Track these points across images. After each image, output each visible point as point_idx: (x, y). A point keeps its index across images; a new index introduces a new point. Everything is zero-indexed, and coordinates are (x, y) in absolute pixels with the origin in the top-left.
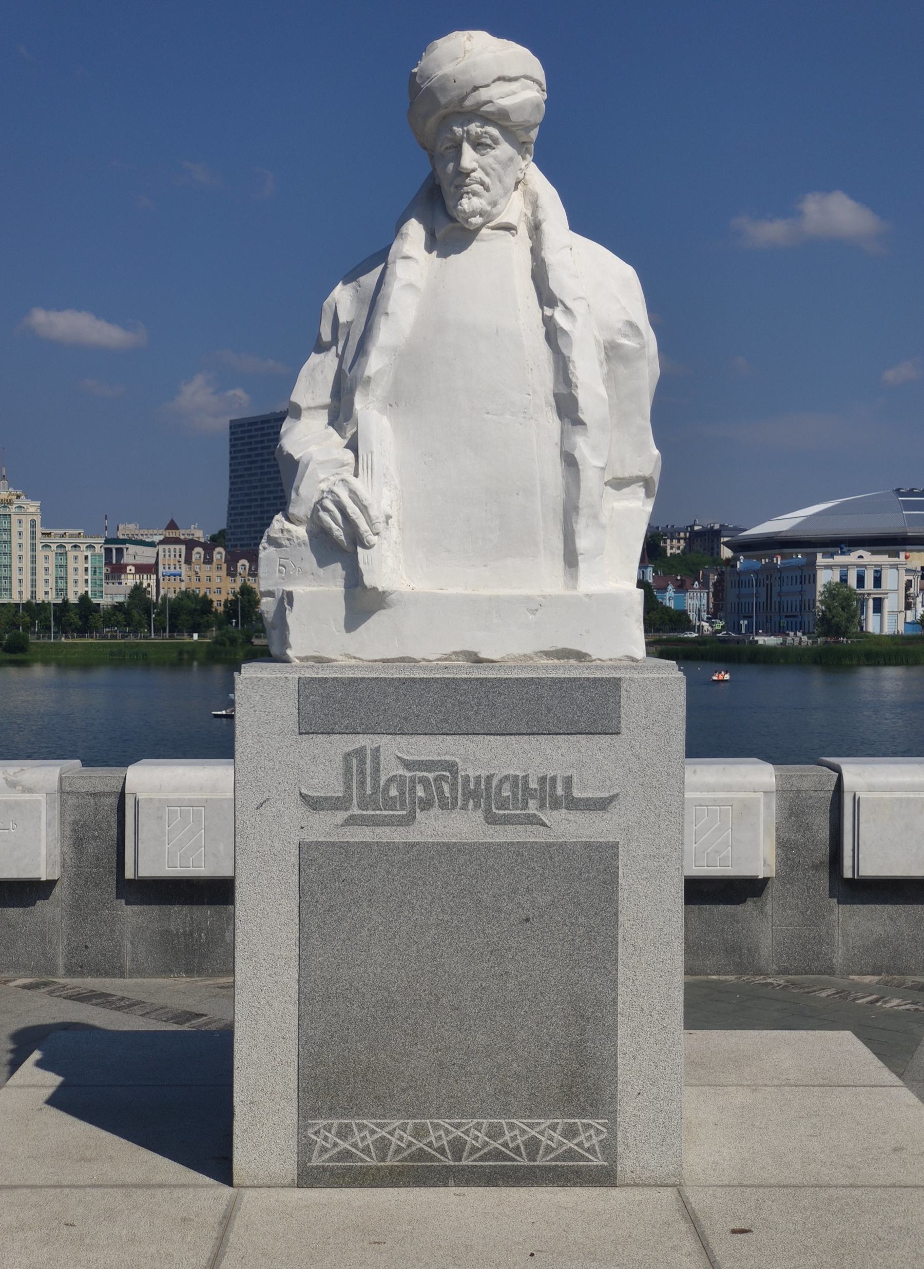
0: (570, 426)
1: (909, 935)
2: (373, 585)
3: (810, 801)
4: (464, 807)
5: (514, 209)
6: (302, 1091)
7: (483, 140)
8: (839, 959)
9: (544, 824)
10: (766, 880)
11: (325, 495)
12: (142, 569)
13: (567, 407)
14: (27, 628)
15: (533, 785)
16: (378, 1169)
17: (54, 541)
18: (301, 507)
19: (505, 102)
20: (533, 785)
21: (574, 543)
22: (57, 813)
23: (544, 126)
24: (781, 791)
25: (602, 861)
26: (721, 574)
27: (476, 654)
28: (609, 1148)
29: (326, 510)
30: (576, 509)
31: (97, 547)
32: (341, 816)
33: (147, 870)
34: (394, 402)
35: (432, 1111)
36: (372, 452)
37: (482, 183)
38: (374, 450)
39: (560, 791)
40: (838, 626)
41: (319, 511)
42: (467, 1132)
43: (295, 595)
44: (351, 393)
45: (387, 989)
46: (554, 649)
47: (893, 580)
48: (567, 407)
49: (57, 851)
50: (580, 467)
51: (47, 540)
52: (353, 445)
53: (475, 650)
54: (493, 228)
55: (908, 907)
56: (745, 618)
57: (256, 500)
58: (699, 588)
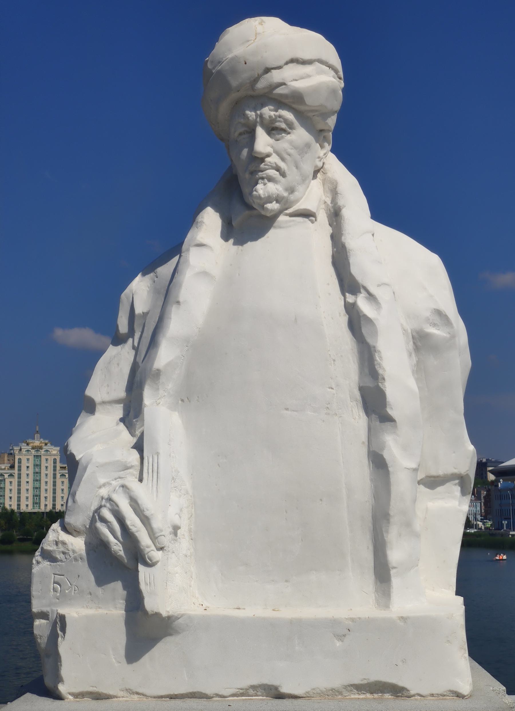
0: (378, 423)
2: (156, 610)
5: (312, 196)
7: (277, 124)
11: (104, 502)
13: (374, 402)
19: (299, 85)
21: (385, 556)
23: (343, 114)
26: (488, 491)
27: (276, 688)
29: (103, 520)
34: (188, 397)
36: (158, 454)
38: (161, 451)
41: (96, 521)
43: (67, 620)
44: (141, 388)
46: (365, 682)
48: (374, 402)
50: (390, 469)
52: (139, 447)
53: (275, 683)
54: (292, 215)
56: (505, 519)
58: (475, 500)
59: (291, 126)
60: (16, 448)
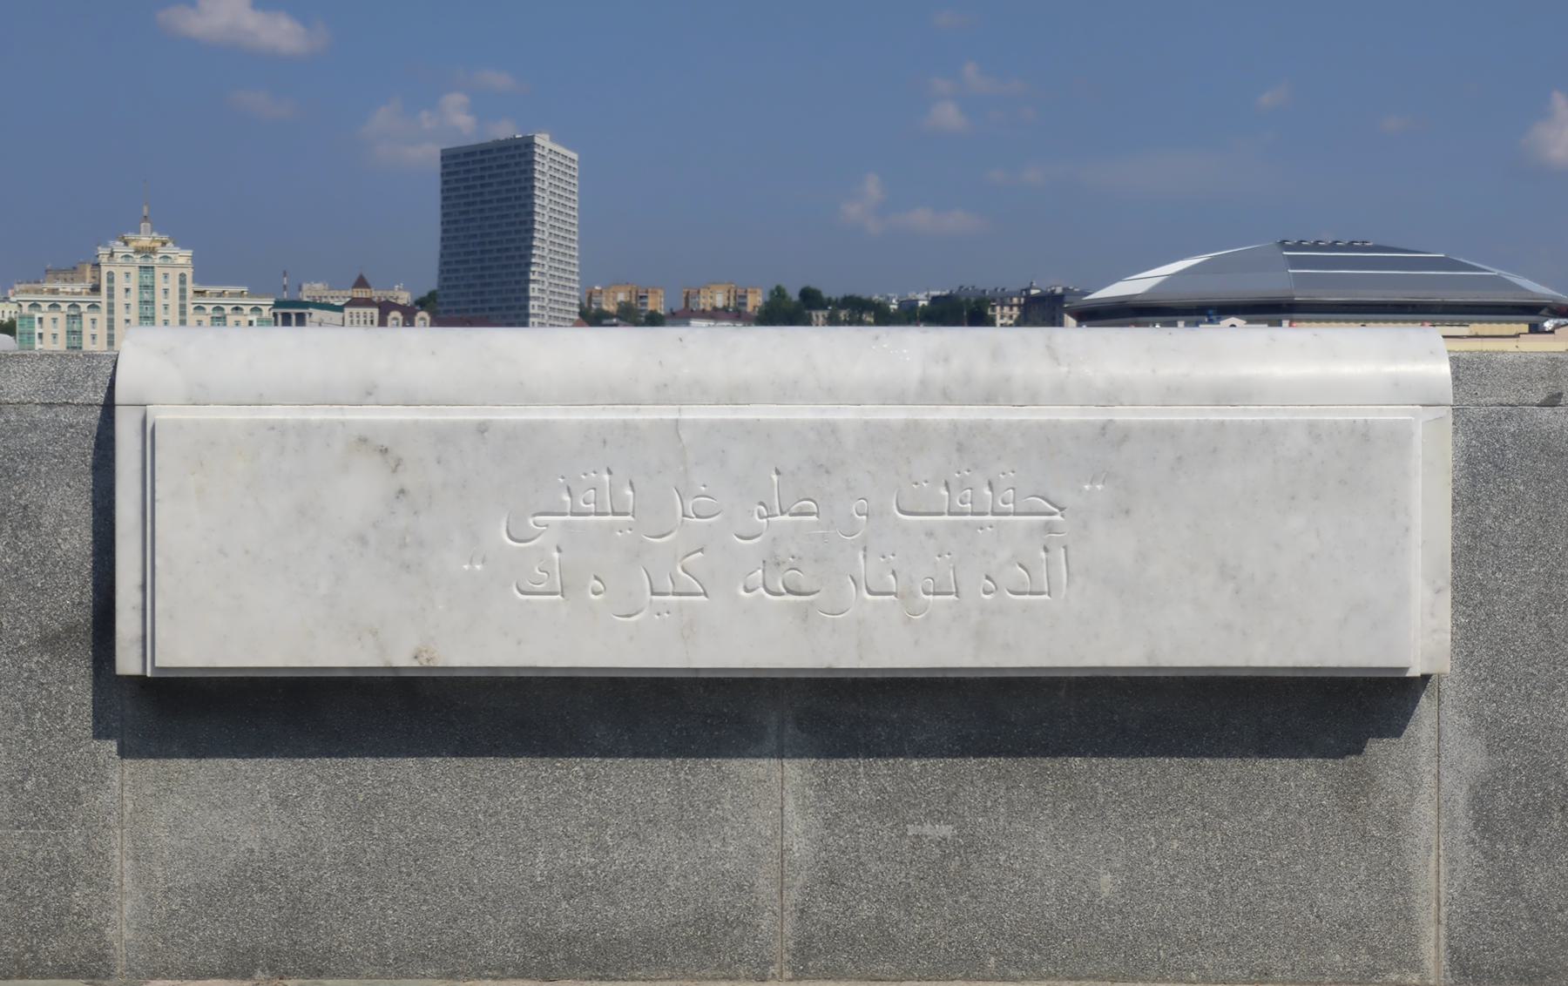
1: (336, 853)
3: (34, 438)
17: (209, 302)
31: (265, 310)
51: (201, 300)
55: (332, 767)
57: (474, 253)
60: (103, 252)
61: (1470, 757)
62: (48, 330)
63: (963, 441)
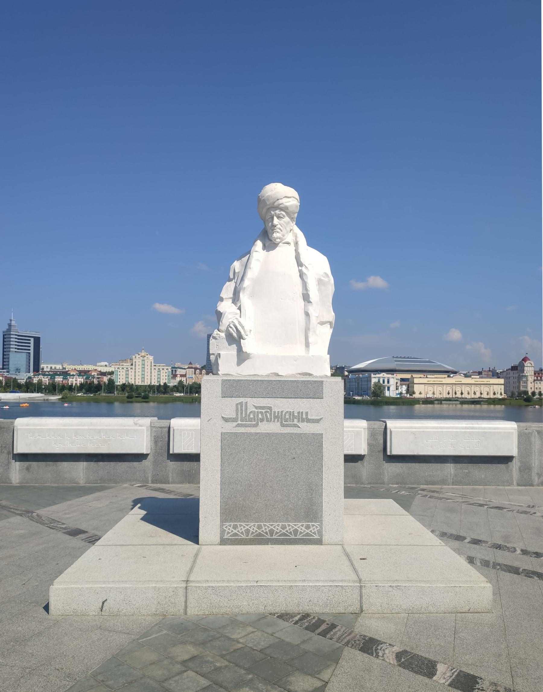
4: (274, 421)
5: (289, 238)
6: (222, 514)
8: (386, 479)
9: (299, 427)
10: (364, 455)
12: (182, 376)
13: (306, 298)
14: (149, 392)
15: (296, 414)
16: (246, 539)
17: (157, 368)
18: (223, 327)
19: (287, 204)
20: (296, 414)
22: (149, 433)
23: (299, 213)
24: (369, 429)
25: (316, 441)
28: (320, 532)
30: (309, 329)
32: (235, 424)
33: (177, 451)
34: (252, 296)
35: (264, 520)
37: (280, 229)
39: (304, 416)
40: (378, 394)
42: (275, 527)
44: (239, 292)
45: (249, 480)
47: (393, 382)
48: (306, 298)
49: (149, 445)
51: (155, 367)
52: (240, 309)
59: (284, 216)
60: (134, 357)
61: (519, 464)
62: (121, 373)
63: (470, 433)
